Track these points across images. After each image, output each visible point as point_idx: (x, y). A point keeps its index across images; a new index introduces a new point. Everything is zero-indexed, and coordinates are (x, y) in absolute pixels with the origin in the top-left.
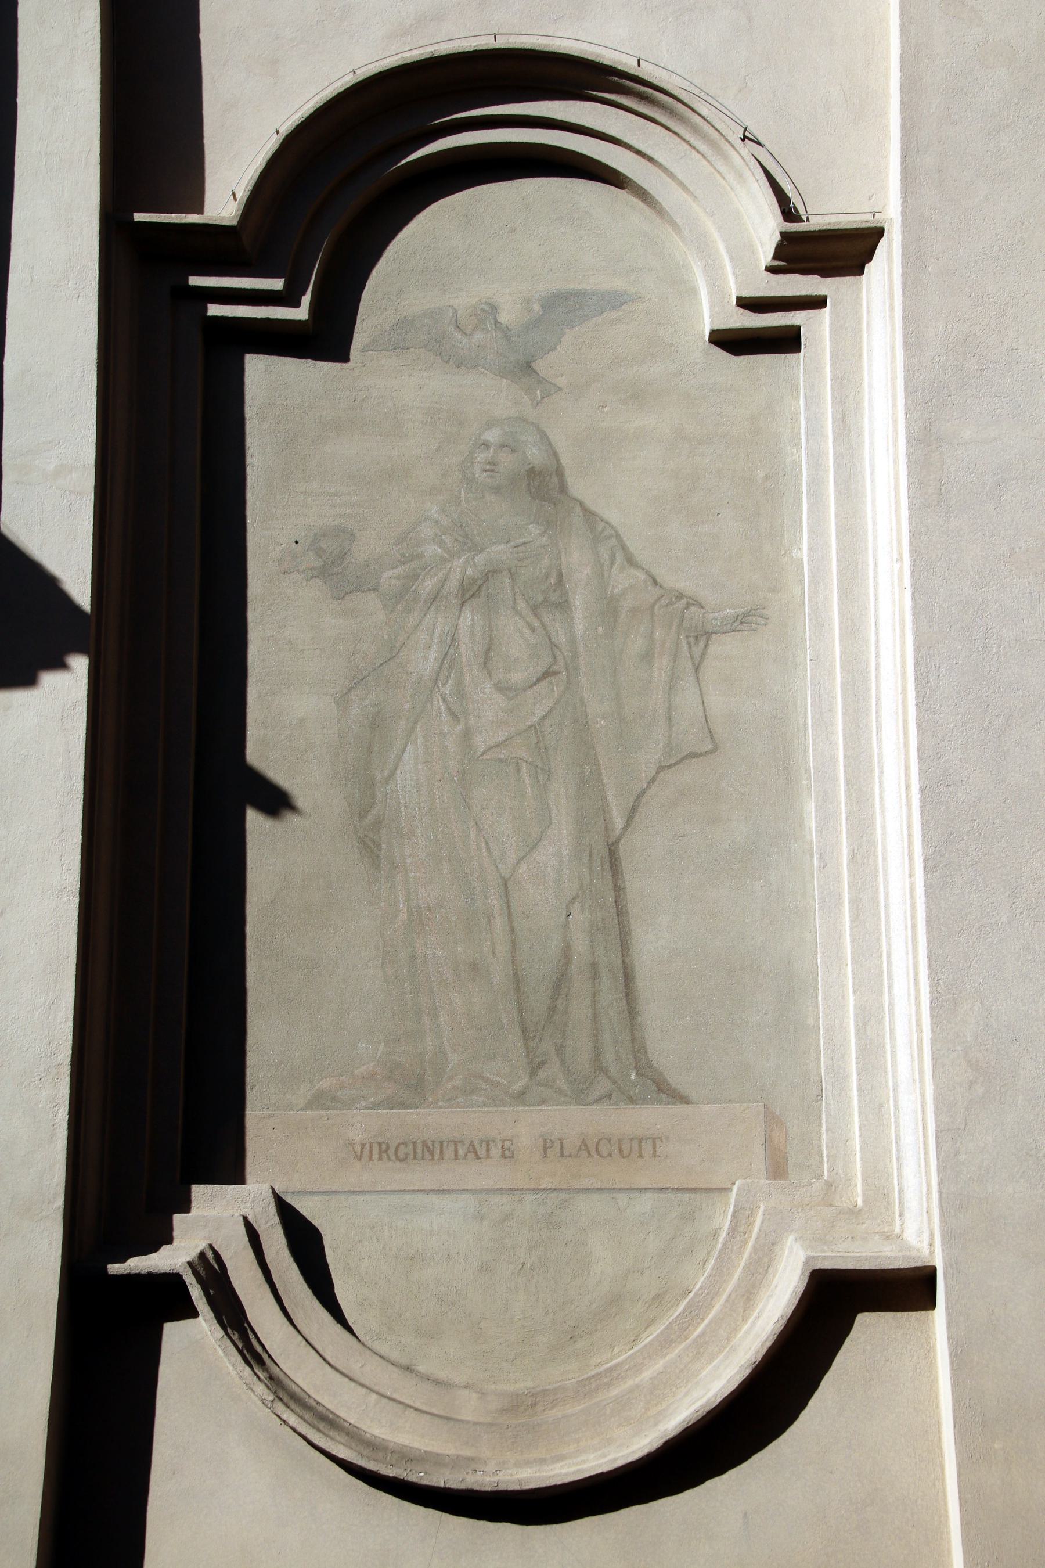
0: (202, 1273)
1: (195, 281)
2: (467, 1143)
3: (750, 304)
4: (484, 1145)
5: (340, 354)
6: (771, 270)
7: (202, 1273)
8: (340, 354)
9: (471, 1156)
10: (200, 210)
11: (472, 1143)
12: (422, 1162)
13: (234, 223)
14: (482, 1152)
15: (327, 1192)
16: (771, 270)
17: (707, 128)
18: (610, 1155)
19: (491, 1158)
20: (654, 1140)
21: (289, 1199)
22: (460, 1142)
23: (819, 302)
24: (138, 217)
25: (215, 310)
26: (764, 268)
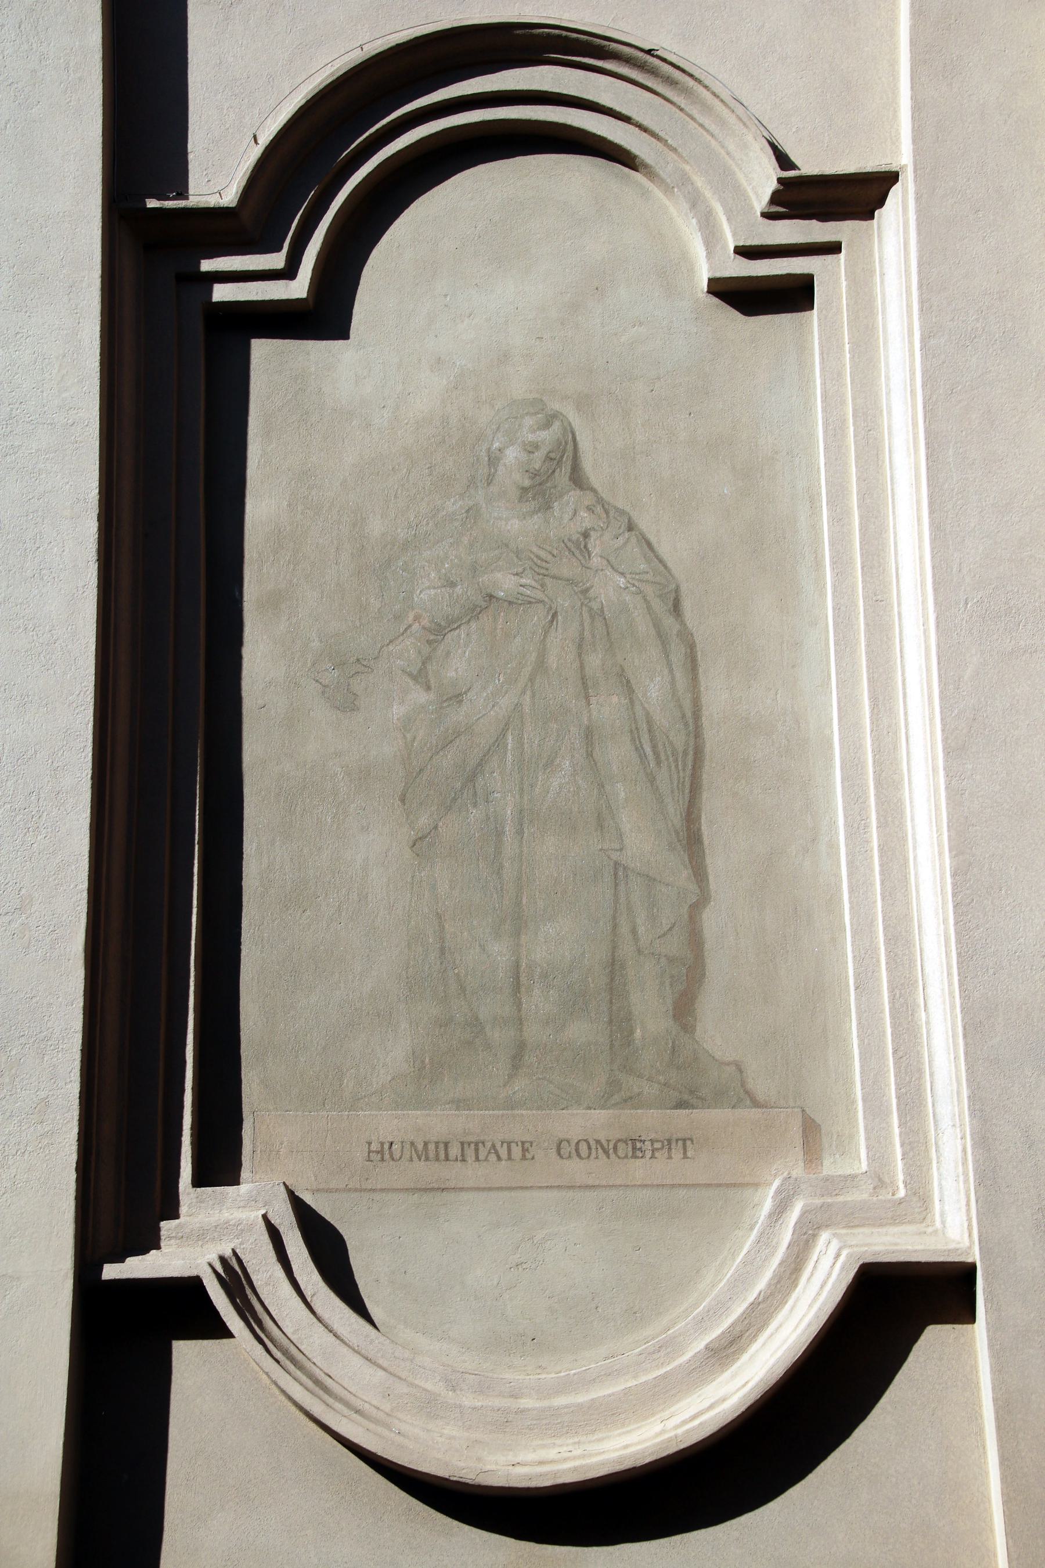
0: (220, 1270)
1: (207, 265)
2: (489, 1145)
3: (748, 252)
4: (505, 1145)
5: (341, 331)
6: (766, 215)
7: (220, 1270)
8: (341, 331)
9: (493, 1157)
10: (183, 194)
11: (493, 1146)
12: (485, 1163)
13: (233, 205)
14: (503, 1152)
15: (432, 1189)
16: (766, 215)
17: (677, 74)
18: (570, 1157)
19: (656, 1158)
20: (477, 1144)
21: (308, 1198)
22: (689, 1139)
23: (833, 248)
24: (152, 203)
25: (222, 293)
26: (759, 214)
